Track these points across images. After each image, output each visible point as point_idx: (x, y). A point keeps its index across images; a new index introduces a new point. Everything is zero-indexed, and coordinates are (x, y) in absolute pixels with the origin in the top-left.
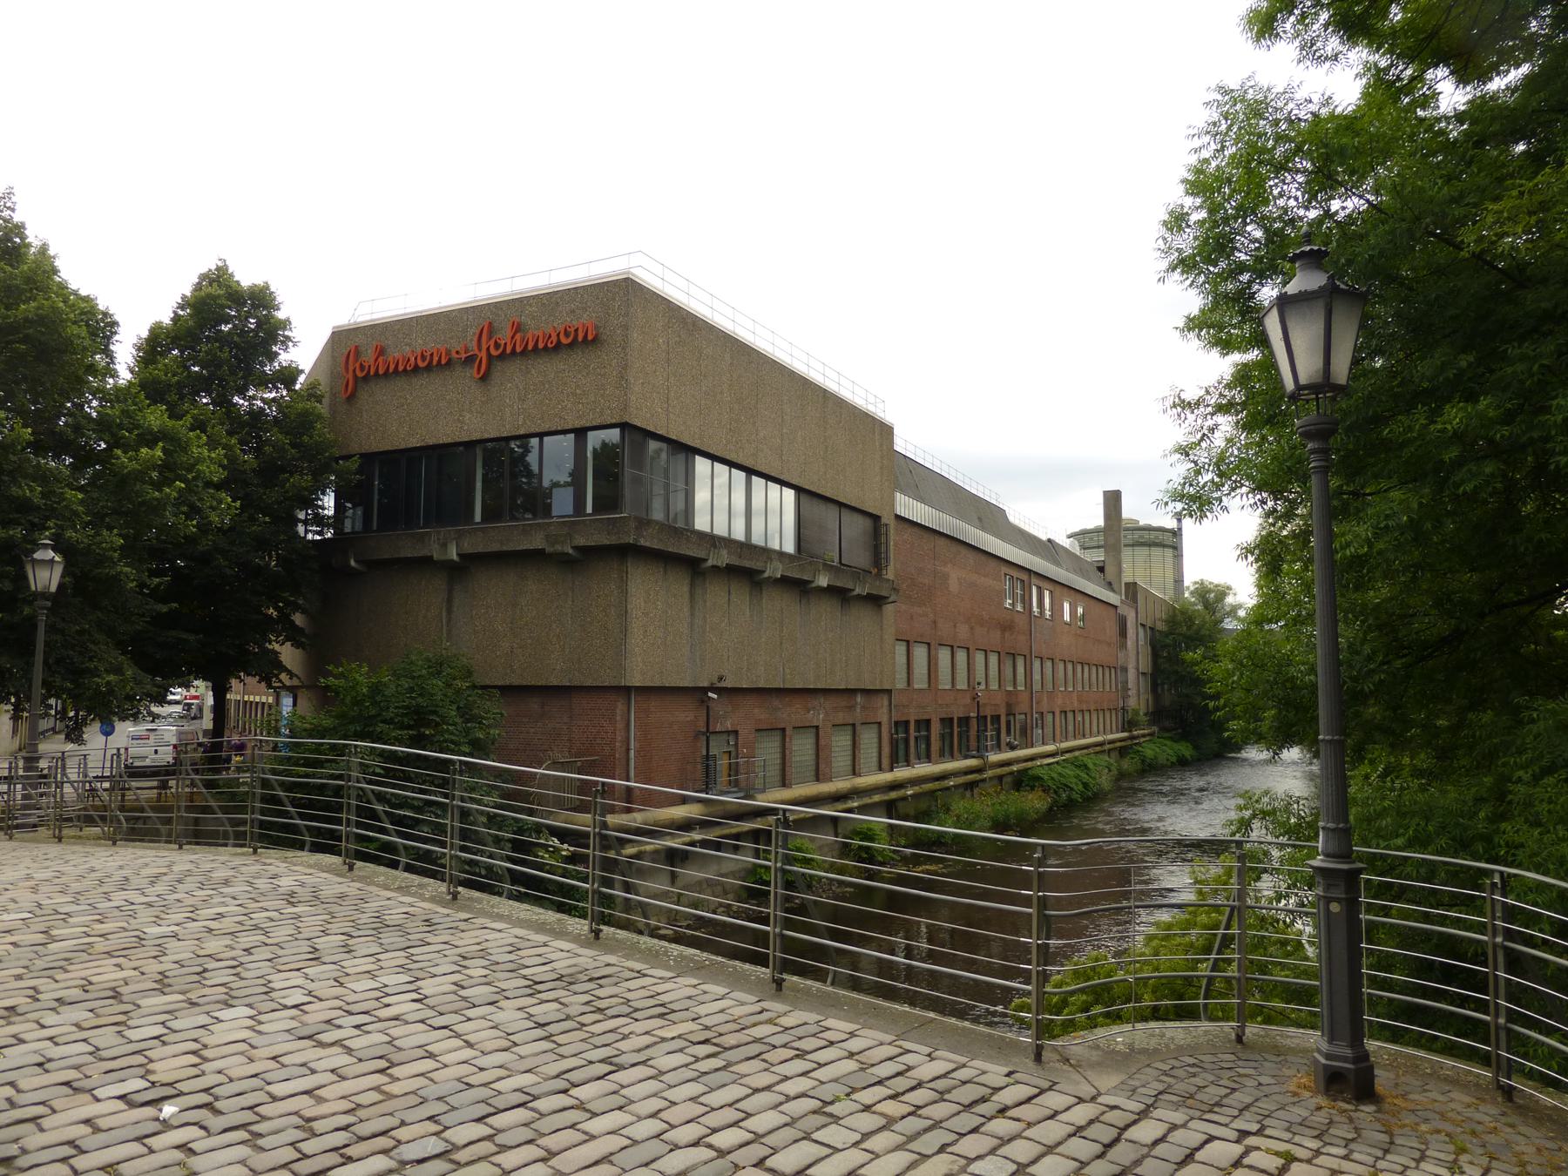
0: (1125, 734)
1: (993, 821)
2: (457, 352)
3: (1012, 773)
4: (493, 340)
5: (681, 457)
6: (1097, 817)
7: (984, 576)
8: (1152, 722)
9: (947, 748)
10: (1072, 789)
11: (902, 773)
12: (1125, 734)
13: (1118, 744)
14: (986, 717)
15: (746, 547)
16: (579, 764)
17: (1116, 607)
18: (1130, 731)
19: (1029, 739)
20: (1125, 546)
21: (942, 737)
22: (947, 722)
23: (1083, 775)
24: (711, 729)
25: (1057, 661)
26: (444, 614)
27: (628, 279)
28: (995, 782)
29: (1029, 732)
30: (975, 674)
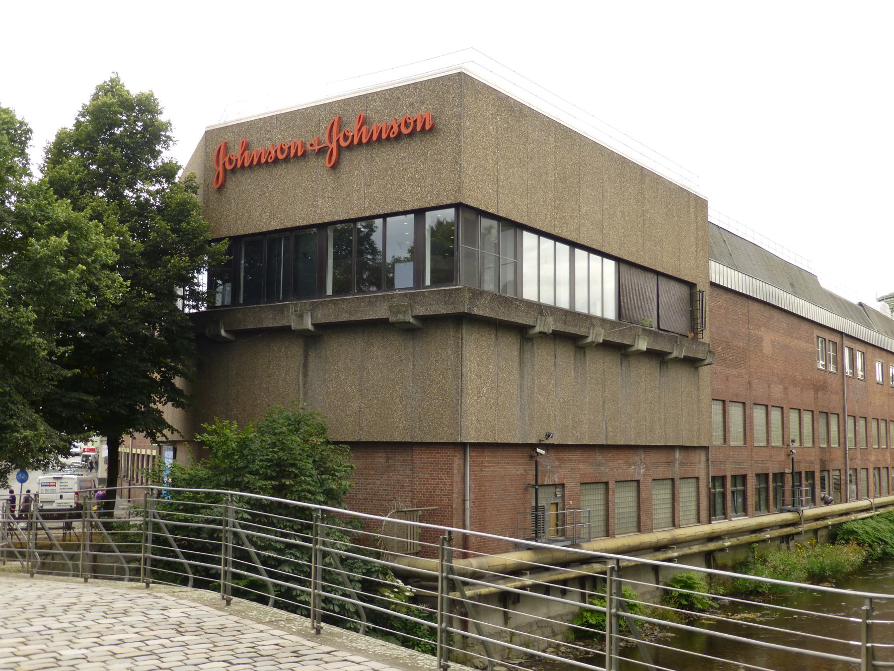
1: (809, 573)
2: (311, 145)
3: (826, 527)
5: (510, 233)
7: (797, 339)
10: (886, 543)
11: (719, 525)
14: (800, 473)
15: (571, 314)
16: (420, 513)
21: (759, 491)
22: (763, 477)
24: (540, 483)
25: (869, 419)
26: (301, 377)
27: (460, 74)
28: (811, 535)
30: (789, 428)
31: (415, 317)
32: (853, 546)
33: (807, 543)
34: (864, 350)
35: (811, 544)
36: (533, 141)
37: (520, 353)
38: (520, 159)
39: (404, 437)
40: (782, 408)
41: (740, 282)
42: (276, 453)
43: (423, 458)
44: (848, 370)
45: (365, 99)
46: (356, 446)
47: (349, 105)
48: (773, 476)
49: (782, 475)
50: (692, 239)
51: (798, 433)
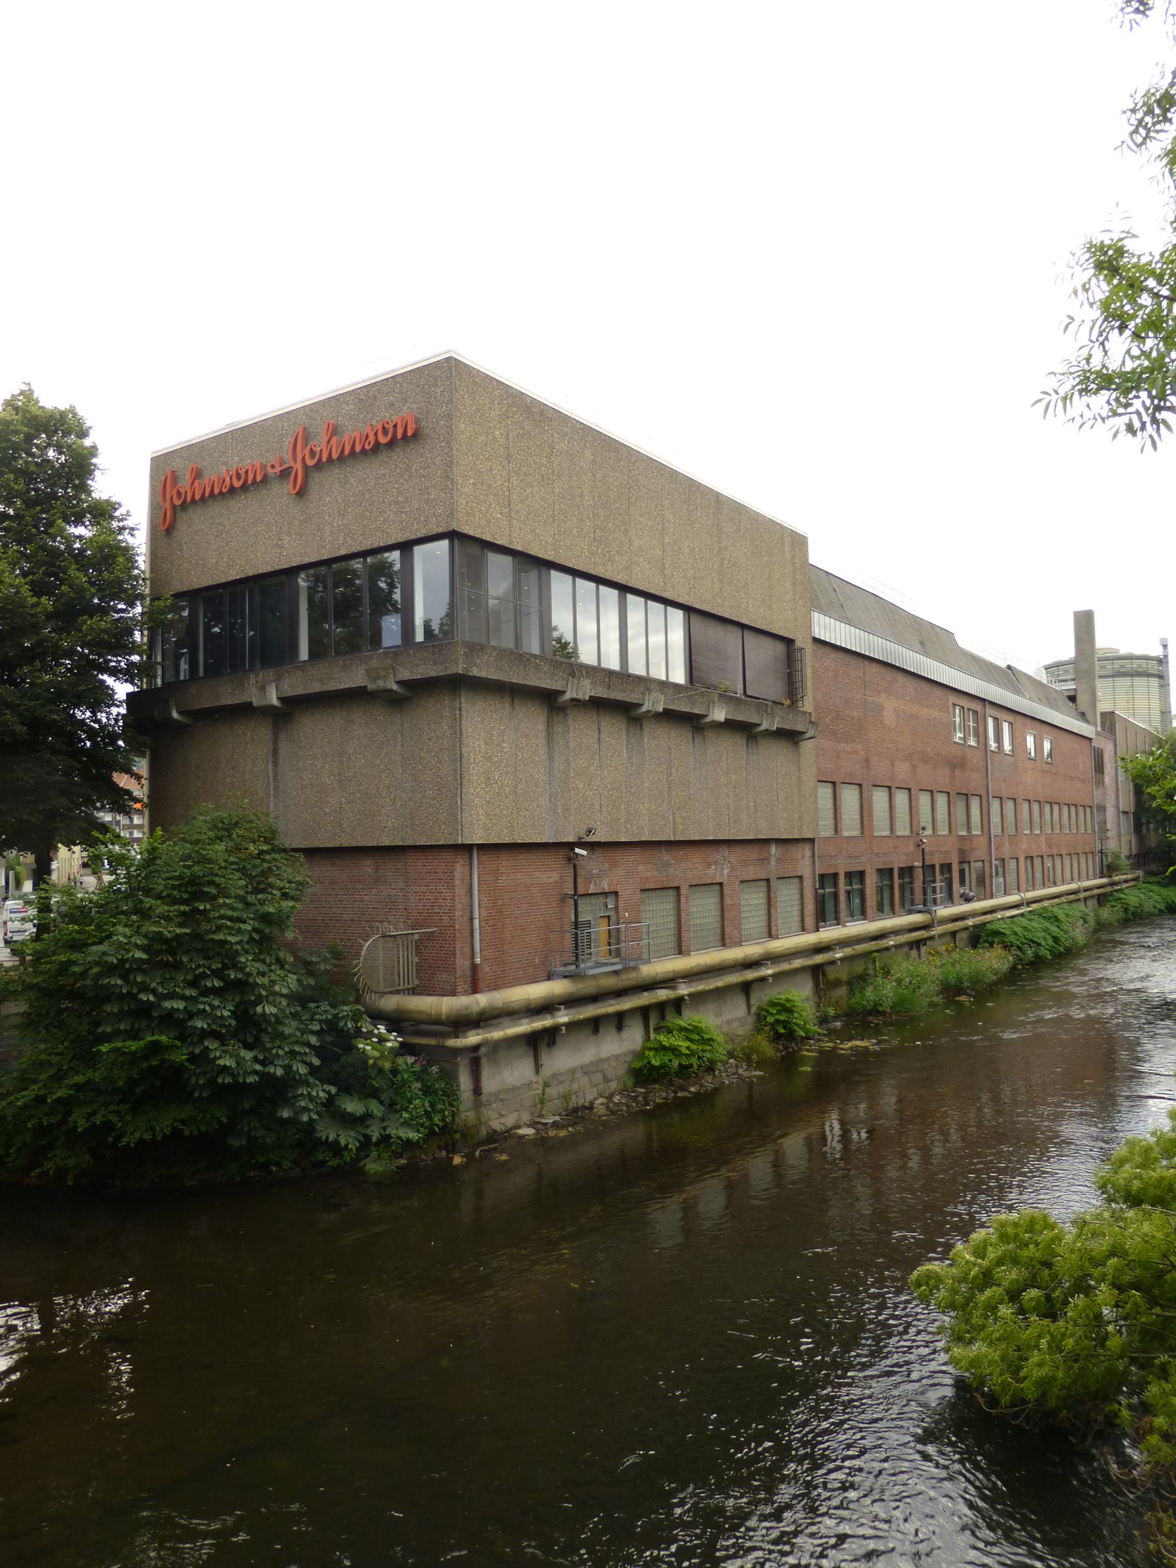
0: (1104, 880)
1: (942, 984)
2: (273, 466)
3: (966, 929)
4: (308, 447)
5: (533, 576)
6: (1068, 978)
7: (928, 707)
8: (1135, 866)
9: (886, 902)
10: (1039, 944)
11: (829, 933)
12: (1104, 880)
13: (1096, 892)
14: (933, 866)
15: (623, 677)
16: (416, 937)
17: (1091, 739)
18: (1110, 876)
19: (988, 890)
20: (1100, 677)
21: (880, 890)
22: (886, 873)
23: (1054, 929)
24: (581, 891)
25: (1020, 800)
26: (270, 768)
27: (450, 358)
28: (949, 938)
29: (987, 880)
30: (918, 814)
31: (399, 683)
32: (998, 950)
33: (942, 949)
34: (1012, 720)
35: (947, 950)
36: (561, 453)
37: (548, 726)
38: (542, 476)
39: (394, 839)
40: (909, 790)
41: (853, 637)
42: (188, 867)
43: (418, 865)
44: (993, 745)
45: (337, 401)
46: (312, 853)
47: (317, 411)
48: (845, 878)
49: (911, 869)
50: (788, 585)
51: (930, 819)
